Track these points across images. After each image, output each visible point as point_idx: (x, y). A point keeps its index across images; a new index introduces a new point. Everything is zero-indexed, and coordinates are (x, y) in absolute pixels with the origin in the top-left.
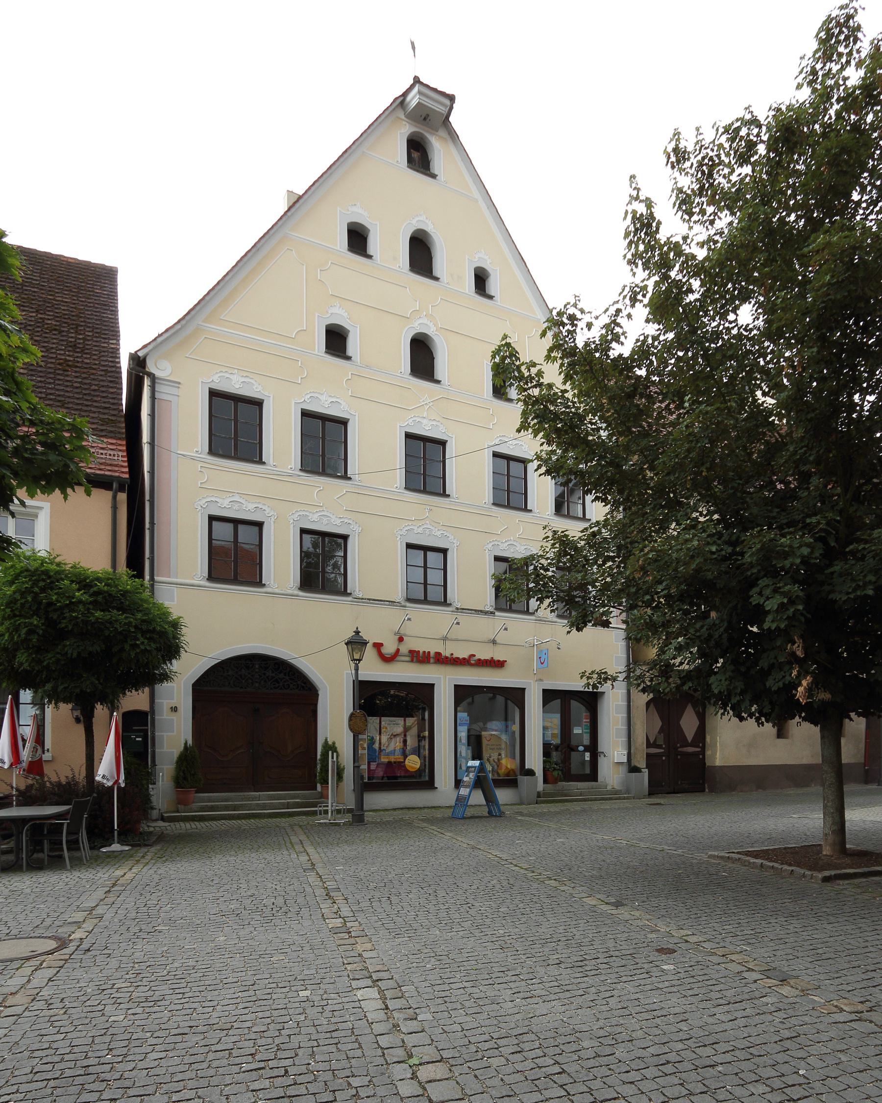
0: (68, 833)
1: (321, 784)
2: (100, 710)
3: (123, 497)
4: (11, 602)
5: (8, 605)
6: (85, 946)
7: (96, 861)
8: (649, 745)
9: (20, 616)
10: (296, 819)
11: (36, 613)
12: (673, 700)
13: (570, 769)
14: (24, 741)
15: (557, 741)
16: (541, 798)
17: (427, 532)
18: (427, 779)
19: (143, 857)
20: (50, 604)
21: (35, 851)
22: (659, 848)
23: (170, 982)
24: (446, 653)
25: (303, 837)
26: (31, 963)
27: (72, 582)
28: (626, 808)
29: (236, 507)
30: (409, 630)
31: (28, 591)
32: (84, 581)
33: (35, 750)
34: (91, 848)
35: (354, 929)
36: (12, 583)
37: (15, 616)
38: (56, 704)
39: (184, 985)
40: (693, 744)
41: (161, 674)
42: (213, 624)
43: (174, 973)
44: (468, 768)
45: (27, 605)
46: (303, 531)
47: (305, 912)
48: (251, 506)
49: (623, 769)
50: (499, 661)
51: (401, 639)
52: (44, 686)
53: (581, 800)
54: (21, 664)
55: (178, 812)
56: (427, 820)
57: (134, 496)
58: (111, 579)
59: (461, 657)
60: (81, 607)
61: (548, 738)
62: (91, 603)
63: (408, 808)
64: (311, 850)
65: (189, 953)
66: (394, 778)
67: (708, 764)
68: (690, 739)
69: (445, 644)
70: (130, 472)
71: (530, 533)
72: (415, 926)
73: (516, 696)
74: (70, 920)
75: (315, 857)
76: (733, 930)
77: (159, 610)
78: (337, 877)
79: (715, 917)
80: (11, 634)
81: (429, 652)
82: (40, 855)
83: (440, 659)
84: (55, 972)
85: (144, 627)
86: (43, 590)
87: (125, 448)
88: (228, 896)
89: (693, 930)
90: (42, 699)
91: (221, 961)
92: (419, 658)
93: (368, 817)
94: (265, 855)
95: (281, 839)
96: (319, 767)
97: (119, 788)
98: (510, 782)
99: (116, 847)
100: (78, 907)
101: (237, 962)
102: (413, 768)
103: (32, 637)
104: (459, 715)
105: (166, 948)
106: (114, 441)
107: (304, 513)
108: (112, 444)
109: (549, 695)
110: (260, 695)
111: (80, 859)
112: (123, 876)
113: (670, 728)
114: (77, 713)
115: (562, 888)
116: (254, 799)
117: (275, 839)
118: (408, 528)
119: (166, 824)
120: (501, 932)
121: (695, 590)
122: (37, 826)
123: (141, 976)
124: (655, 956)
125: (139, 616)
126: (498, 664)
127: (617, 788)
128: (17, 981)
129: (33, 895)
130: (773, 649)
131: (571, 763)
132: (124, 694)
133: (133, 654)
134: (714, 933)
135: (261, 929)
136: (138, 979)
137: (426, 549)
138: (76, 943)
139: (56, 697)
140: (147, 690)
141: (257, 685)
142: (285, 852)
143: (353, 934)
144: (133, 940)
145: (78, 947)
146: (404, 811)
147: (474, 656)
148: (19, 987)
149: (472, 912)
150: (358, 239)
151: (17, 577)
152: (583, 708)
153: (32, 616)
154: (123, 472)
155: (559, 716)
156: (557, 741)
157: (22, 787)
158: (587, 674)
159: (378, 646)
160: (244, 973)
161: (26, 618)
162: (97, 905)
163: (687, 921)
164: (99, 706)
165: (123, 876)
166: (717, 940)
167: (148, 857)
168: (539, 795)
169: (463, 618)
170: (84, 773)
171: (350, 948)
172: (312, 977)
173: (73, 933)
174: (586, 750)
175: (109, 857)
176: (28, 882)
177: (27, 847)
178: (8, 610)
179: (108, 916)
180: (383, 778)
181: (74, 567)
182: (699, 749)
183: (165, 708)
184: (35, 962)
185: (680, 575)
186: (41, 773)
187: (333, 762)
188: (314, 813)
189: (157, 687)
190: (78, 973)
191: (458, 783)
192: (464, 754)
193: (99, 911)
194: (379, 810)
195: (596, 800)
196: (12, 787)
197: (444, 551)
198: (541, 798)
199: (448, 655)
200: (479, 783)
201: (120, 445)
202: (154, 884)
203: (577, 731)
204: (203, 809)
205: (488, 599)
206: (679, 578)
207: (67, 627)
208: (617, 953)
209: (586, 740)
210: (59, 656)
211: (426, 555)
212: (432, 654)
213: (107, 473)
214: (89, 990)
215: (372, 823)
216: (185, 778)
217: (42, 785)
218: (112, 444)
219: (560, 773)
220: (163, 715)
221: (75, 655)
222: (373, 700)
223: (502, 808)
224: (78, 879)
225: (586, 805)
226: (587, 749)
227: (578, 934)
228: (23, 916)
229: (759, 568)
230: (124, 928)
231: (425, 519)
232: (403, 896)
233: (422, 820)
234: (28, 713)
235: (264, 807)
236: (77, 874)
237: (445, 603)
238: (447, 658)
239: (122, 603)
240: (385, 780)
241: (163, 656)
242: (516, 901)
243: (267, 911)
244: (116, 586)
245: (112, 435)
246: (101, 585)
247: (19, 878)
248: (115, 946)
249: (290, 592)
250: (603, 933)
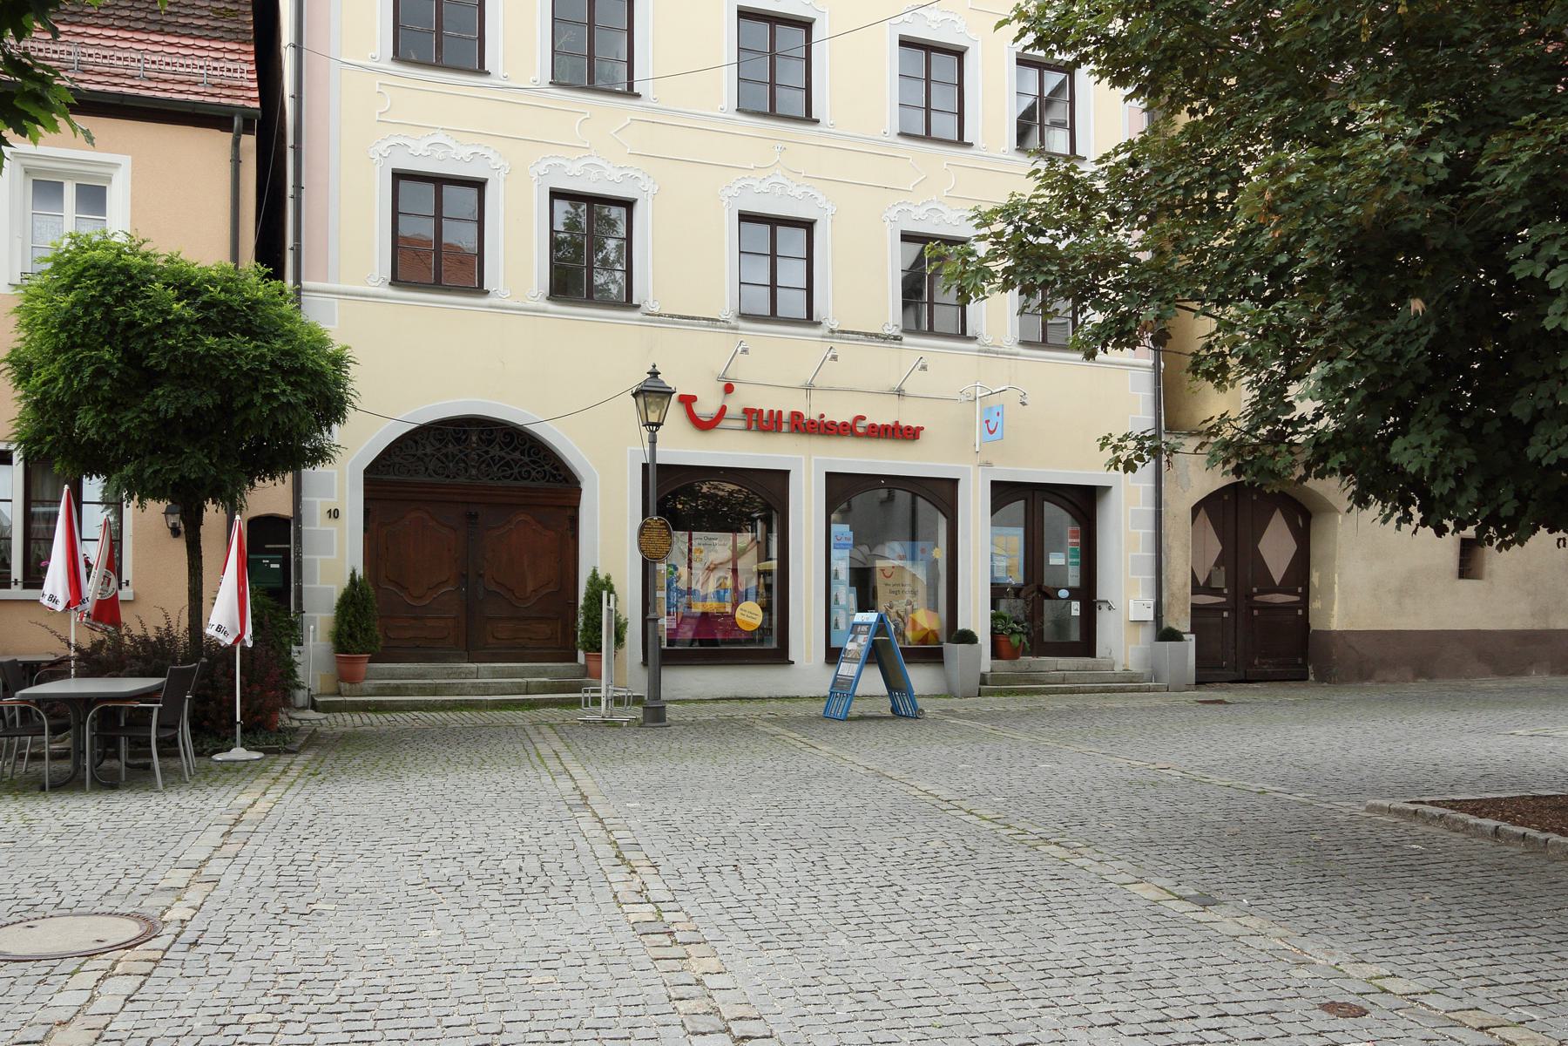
0: (160, 726)
1: (586, 650)
2: (213, 514)
3: (249, 142)
4: (68, 322)
5: (63, 326)
6: (189, 936)
7: (206, 777)
8: (1196, 589)
9: (83, 345)
10: (543, 713)
11: (108, 341)
12: (1254, 501)
13: (1041, 632)
14: (88, 565)
15: (1017, 578)
16: (987, 685)
17: (778, 190)
18: (774, 645)
19: (284, 772)
20: (132, 324)
21: (105, 756)
22: (1254, 787)
23: (343, 1017)
24: (811, 414)
25: (558, 746)
26: (92, 964)
27: (168, 285)
28: (1158, 708)
29: (439, 154)
30: (742, 371)
31: (96, 302)
32: (187, 286)
33: (106, 580)
34: (198, 754)
35: (680, 926)
36: (68, 289)
37: (74, 345)
38: (140, 500)
39: (370, 1025)
40: (1285, 588)
41: (315, 449)
42: (403, 365)
43: (349, 999)
44: (855, 625)
45: (94, 327)
46: (555, 194)
47: (580, 888)
48: (465, 152)
49: (1148, 633)
50: (909, 428)
51: (729, 389)
52: (121, 469)
53: (1064, 691)
54: (85, 430)
55: (339, 694)
56: (776, 721)
57: (266, 132)
58: (231, 280)
59: (839, 421)
60: (182, 328)
61: (1000, 574)
62: (198, 321)
63: (741, 699)
64: (576, 770)
65: (374, 960)
66: (711, 642)
67: (1315, 625)
68: (1277, 579)
69: (808, 396)
70: (262, 99)
71: (980, 182)
72: (797, 926)
73: (943, 493)
74: (163, 884)
75: (587, 784)
76: (1484, 971)
77: (310, 334)
78: (631, 822)
79: (1430, 940)
80: (68, 378)
81: (780, 413)
82: (114, 763)
83: (801, 426)
84: (137, 984)
85: (286, 364)
86: (120, 300)
87: (252, 58)
88: (436, 851)
89: (1390, 966)
90: (118, 492)
91: (435, 978)
92: (762, 422)
93: (672, 711)
94: (497, 777)
95: (519, 747)
96: (581, 620)
97: (243, 648)
98: (928, 653)
99: (238, 753)
100: (177, 859)
101: (464, 982)
102: (749, 624)
103: (102, 382)
104: (835, 528)
105: (332, 947)
106: (235, 47)
107: (557, 161)
108: (232, 51)
109: (1003, 493)
110: (479, 497)
111: (179, 773)
112: (252, 806)
113: (1238, 554)
114: (175, 519)
115: (1078, 862)
116: (459, 675)
117: (509, 747)
118: (743, 183)
119: (321, 715)
120: (974, 947)
121: (1373, 260)
122: (108, 712)
123: (291, 1000)
124: (1321, 1020)
125: (278, 344)
126: (910, 434)
127: (1134, 668)
128: (71, 999)
129: (101, 835)
130: (1545, 377)
131: (1046, 622)
132: (252, 484)
133: (266, 411)
134: (1442, 975)
135: (502, 917)
136: (286, 1006)
137: (774, 222)
138: (173, 929)
139: (145, 489)
140: (289, 477)
141: (474, 472)
142: (531, 772)
143: (679, 937)
144: (273, 929)
145: (177, 936)
146: (734, 704)
147: (863, 418)
148: (75, 1010)
149: (903, 902)
151: (79, 276)
152: (1067, 517)
153: (102, 345)
154: (250, 99)
155: (1020, 531)
156: (1017, 578)
157: (86, 645)
158: (1114, 440)
159: (688, 401)
160: (479, 1008)
161: (90, 348)
162: (209, 858)
163: (1368, 946)
164: (210, 507)
165: (252, 806)
166: (1454, 992)
167: (293, 773)
168: (983, 680)
169: (842, 347)
170: (185, 622)
171: (676, 965)
172: (611, 1022)
173: (169, 908)
174: (1072, 597)
175: (227, 770)
176: (93, 811)
177: (92, 749)
178: (63, 336)
179: (226, 881)
180: (692, 642)
181: (170, 261)
182: (1296, 598)
184: (102, 963)
185: (1347, 222)
186: (115, 621)
187: (610, 610)
188: (576, 703)
189: (307, 472)
190: (179, 988)
191: (833, 655)
192: (842, 601)
193: (214, 868)
194: (689, 701)
195: (1092, 691)
196: (69, 644)
197: (808, 225)
198: (987, 685)
199: (815, 417)
200: (876, 654)
201: (246, 52)
202: (304, 822)
203: (1056, 559)
204: (381, 691)
205: (888, 310)
206: (1347, 228)
207: (158, 364)
208: (1234, 1009)
209: (1074, 579)
210: (145, 416)
211: (774, 231)
212: (785, 417)
213: (224, 101)
214: (197, 1025)
215: (679, 723)
216: (351, 636)
217: (118, 641)
218: (232, 51)
219: (1024, 639)
220: (315, 525)
221: (171, 412)
222: (683, 501)
223: (919, 702)
224: (175, 809)
225: (1077, 700)
226: (1074, 594)
227: (1137, 960)
228: (83, 873)
229: (1527, 202)
230: (257, 903)
231: (776, 168)
232: (762, 864)
233: (768, 720)
234: (95, 518)
235: (486, 690)
236: (173, 798)
237: (809, 320)
238: (812, 422)
239: (250, 321)
240: (696, 647)
241: (317, 417)
242: (989, 885)
243: (510, 882)
244: (240, 293)
245: (233, 36)
246: (215, 291)
247: (80, 803)
248: (241, 939)
249: (532, 304)
250: (1191, 963)
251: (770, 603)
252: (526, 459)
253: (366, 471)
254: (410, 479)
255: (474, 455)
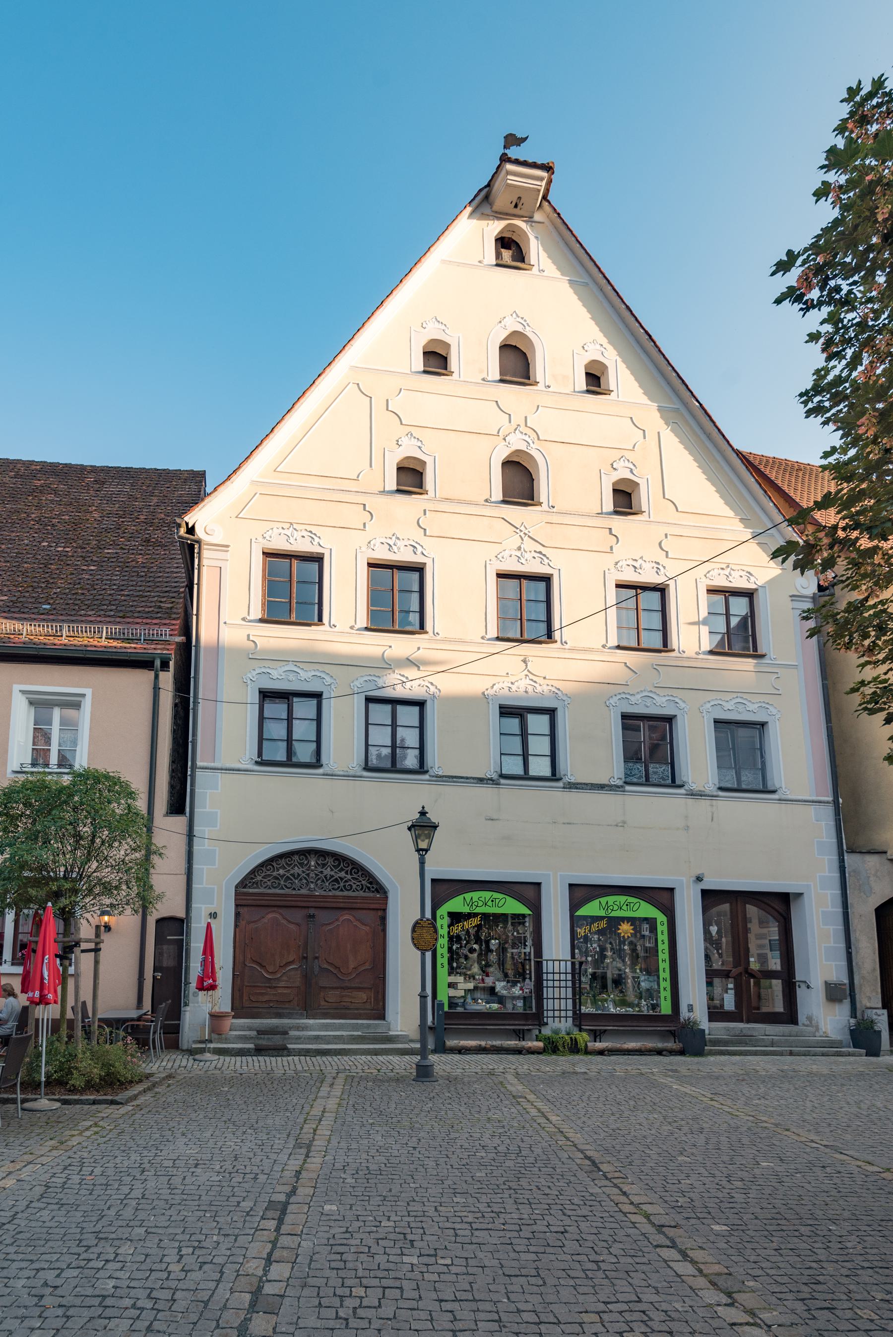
107: (370, 678)
109: (710, 897)
150: (437, 360)
183: (203, 913)
205: (610, 764)
235: (317, 1039)
251: (185, 985)
252: (349, 877)
253: (236, 887)
254: (251, 891)
255: (312, 875)
